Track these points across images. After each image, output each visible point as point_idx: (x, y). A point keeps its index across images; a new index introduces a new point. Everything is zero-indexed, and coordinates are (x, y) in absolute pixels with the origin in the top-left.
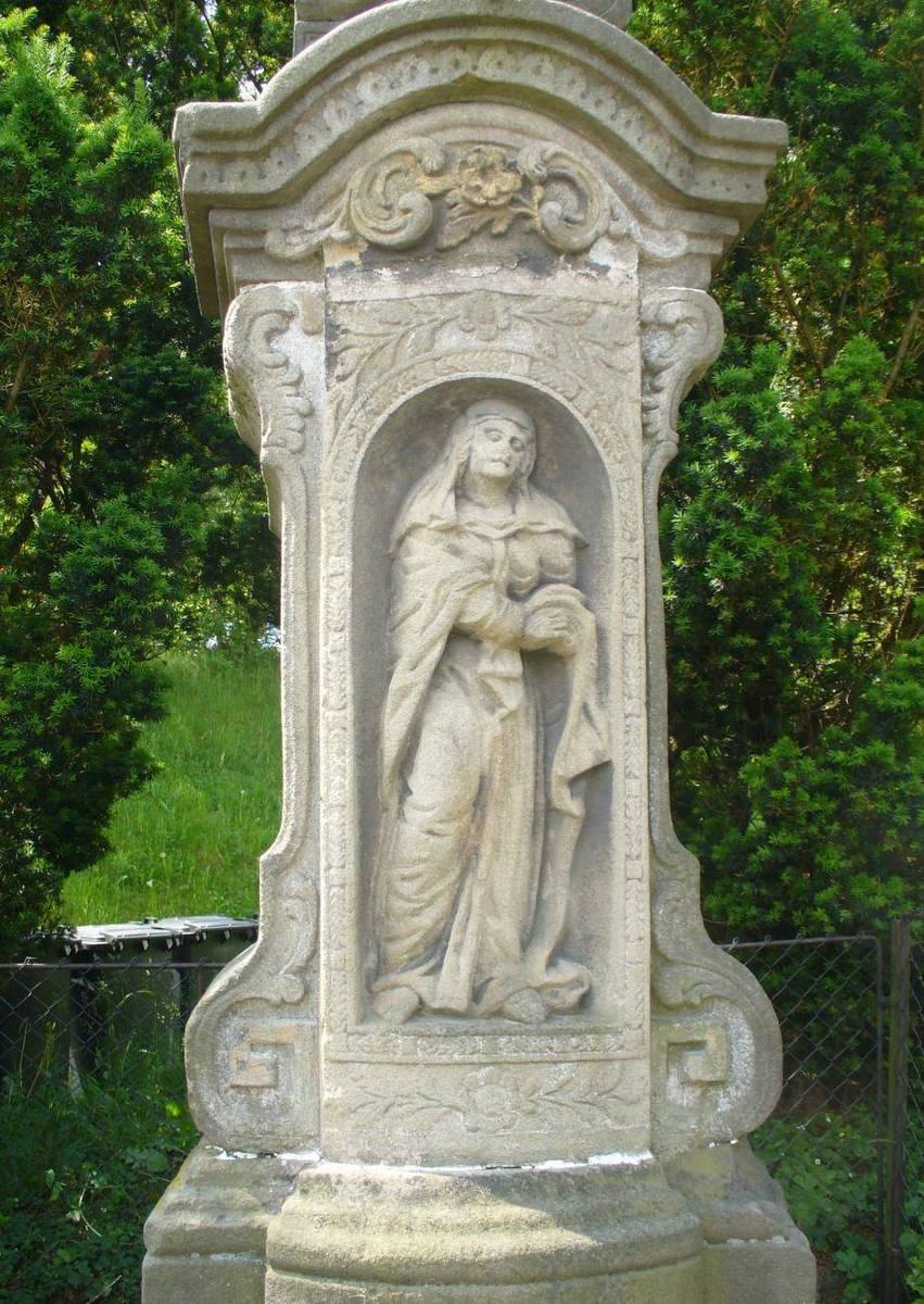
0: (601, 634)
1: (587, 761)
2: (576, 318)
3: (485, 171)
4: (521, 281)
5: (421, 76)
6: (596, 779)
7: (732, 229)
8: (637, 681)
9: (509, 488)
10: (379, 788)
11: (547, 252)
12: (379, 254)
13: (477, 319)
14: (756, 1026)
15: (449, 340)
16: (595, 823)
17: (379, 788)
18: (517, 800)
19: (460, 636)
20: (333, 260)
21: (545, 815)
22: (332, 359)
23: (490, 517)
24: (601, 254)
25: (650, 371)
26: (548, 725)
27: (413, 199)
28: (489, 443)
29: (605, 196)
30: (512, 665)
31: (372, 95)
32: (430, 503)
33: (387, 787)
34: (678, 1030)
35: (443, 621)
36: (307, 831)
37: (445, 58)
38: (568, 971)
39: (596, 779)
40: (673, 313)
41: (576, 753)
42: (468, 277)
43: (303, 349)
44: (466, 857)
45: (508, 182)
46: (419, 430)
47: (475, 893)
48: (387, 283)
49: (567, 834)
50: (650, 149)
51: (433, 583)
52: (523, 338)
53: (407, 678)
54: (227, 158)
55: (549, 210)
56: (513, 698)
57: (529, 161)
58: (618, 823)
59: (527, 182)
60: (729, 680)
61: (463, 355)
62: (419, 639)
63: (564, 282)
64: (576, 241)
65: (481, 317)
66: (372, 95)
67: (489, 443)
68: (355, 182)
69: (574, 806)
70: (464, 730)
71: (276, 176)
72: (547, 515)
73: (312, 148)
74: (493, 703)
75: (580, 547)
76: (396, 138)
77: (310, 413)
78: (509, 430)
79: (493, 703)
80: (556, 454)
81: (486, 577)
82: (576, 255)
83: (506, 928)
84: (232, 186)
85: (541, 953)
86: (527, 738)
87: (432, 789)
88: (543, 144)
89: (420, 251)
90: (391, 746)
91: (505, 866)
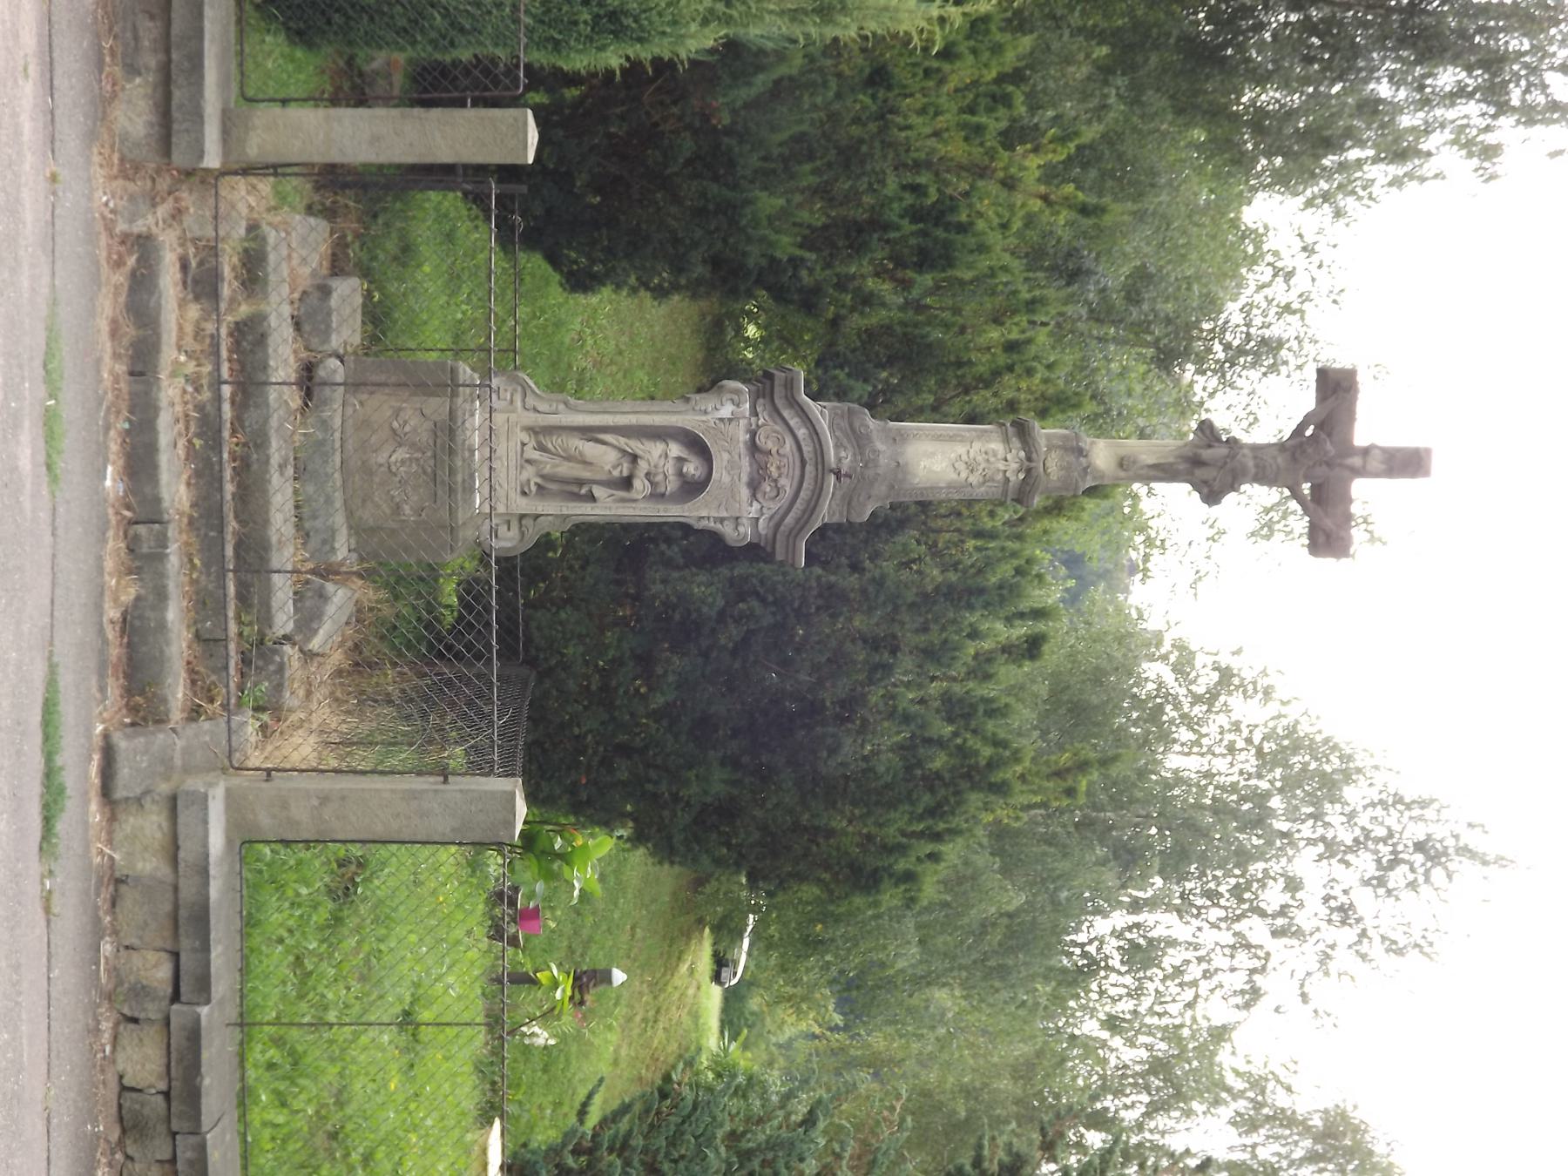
0: (635, 501)
1: (596, 494)
2: (732, 492)
3: (779, 468)
4: (745, 478)
5: (807, 449)
6: (591, 498)
7: (769, 549)
8: (621, 512)
9: (680, 474)
10: (589, 433)
11: (754, 487)
12: (753, 434)
13: (731, 468)
14: (514, 548)
15: (726, 456)
16: (577, 497)
17: (589, 433)
18: (585, 474)
19: (634, 458)
20: (753, 419)
21: (580, 483)
22: (721, 420)
23: (670, 468)
24: (756, 505)
25: (722, 520)
26: (611, 484)
27: (770, 445)
28: (693, 468)
29: (775, 506)
30: (625, 473)
31: (802, 433)
32: (675, 450)
33: (590, 435)
34: (515, 524)
35: (639, 452)
36: (577, 410)
37: (812, 455)
38: (534, 488)
39: (591, 498)
40: (741, 529)
41: (598, 491)
42: (745, 462)
43: (727, 411)
44: (569, 458)
45: (775, 474)
46: (697, 446)
47: (558, 460)
48: (744, 437)
49: (575, 489)
50: (789, 520)
51: (653, 451)
52: (726, 479)
53: (622, 441)
54: (785, 386)
55: (767, 487)
56: (616, 473)
57: (783, 482)
58: (571, 505)
59: (776, 481)
60: (630, 546)
61: (720, 460)
62: (635, 445)
63: (745, 493)
64: (759, 496)
65: (732, 466)
66: (802, 433)
67: (693, 468)
68: (777, 428)
69: (583, 491)
70: (605, 457)
71: (779, 402)
72: (672, 485)
73: (786, 414)
74: (615, 467)
75: (663, 495)
76: (789, 442)
77: (706, 412)
78: (698, 474)
79: (615, 467)
80: (692, 488)
81: (1022, 510)
82: (754, 496)
83: (547, 470)
84: (777, 389)
85: (539, 480)
86: (604, 477)
87: (590, 449)
88: (787, 485)
89: (753, 447)
90: (608, 437)
91: (566, 469)
